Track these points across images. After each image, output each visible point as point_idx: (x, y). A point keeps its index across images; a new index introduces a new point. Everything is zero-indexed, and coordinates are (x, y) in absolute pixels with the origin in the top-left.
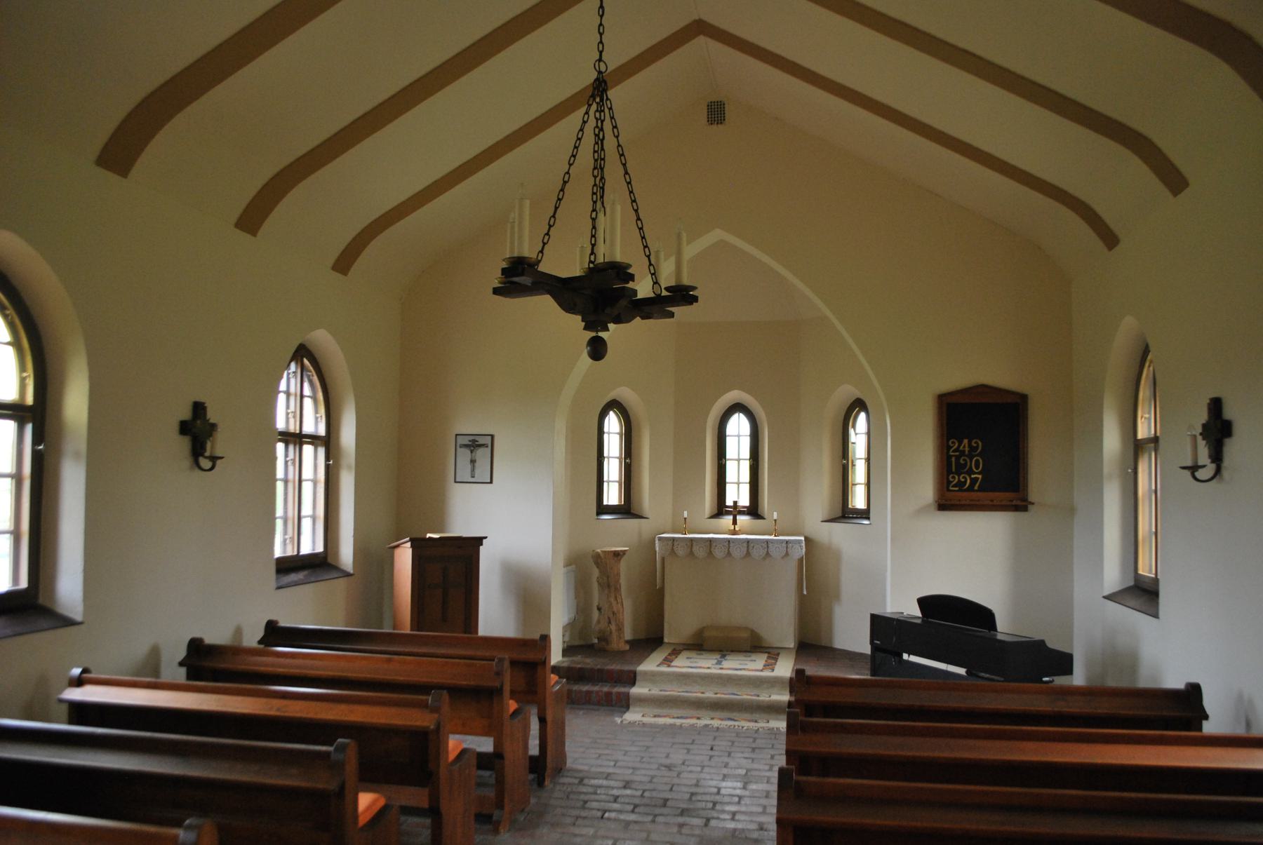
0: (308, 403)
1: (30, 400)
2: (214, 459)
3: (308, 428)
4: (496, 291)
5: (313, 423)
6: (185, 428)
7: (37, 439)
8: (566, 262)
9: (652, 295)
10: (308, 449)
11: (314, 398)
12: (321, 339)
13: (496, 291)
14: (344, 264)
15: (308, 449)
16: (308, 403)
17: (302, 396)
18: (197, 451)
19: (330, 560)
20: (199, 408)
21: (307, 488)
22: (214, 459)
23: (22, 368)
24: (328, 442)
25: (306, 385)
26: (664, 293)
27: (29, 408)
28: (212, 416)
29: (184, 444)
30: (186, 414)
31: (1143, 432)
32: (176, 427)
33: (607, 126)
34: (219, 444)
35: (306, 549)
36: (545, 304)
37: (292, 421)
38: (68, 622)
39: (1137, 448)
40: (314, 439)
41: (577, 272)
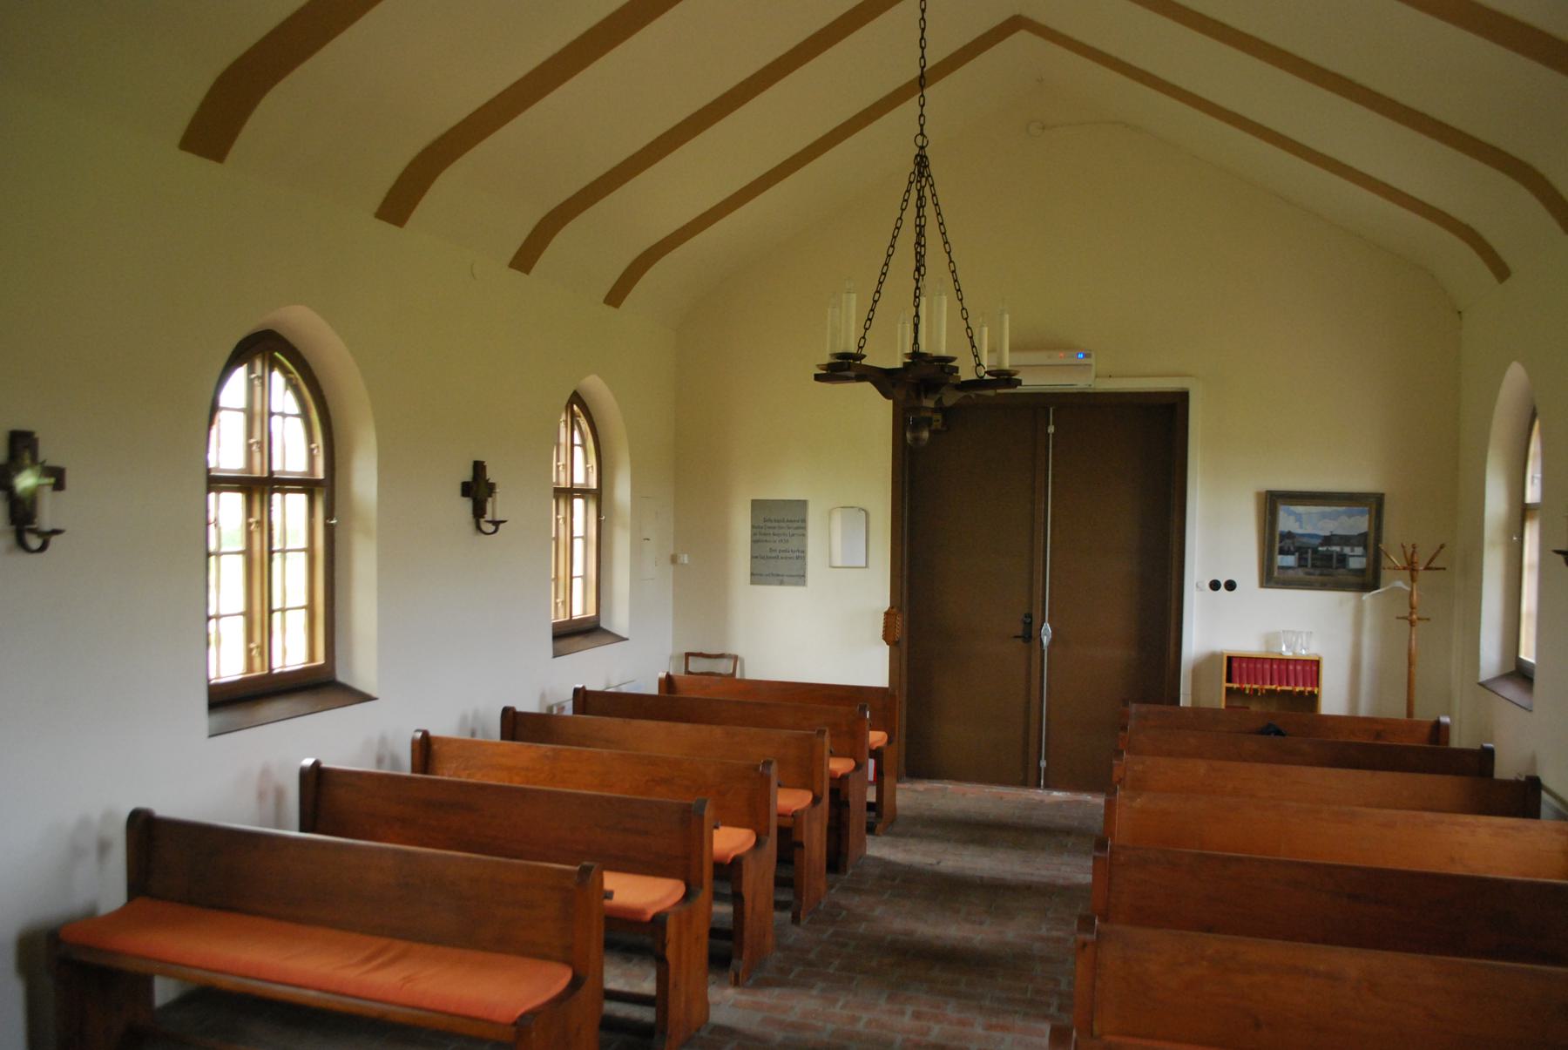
0: (578, 451)
1: (320, 474)
2: (497, 523)
3: (579, 479)
4: (818, 377)
5: (582, 472)
6: (466, 489)
7: (330, 513)
8: (889, 355)
9: (974, 377)
10: (579, 503)
11: (583, 445)
12: (595, 386)
13: (818, 377)
14: (615, 297)
15: (579, 503)
16: (578, 451)
17: (572, 445)
18: (479, 512)
19: (603, 625)
20: (479, 467)
21: (578, 545)
22: (497, 523)
23: (310, 438)
24: (598, 496)
25: (576, 434)
26: (987, 377)
27: (318, 483)
28: (491, 475)
29: (467, 505)
30: (467, 475)
31: (1533, 494)
32: (458, 489)
33: (929, 210)
34: (497, 507)
35: (578, 613)
36: (867, 388)
37: (562, 475)
38: (364, 698)
39: (1521, 512)
40: (584, 492)
41: (899, 365)
